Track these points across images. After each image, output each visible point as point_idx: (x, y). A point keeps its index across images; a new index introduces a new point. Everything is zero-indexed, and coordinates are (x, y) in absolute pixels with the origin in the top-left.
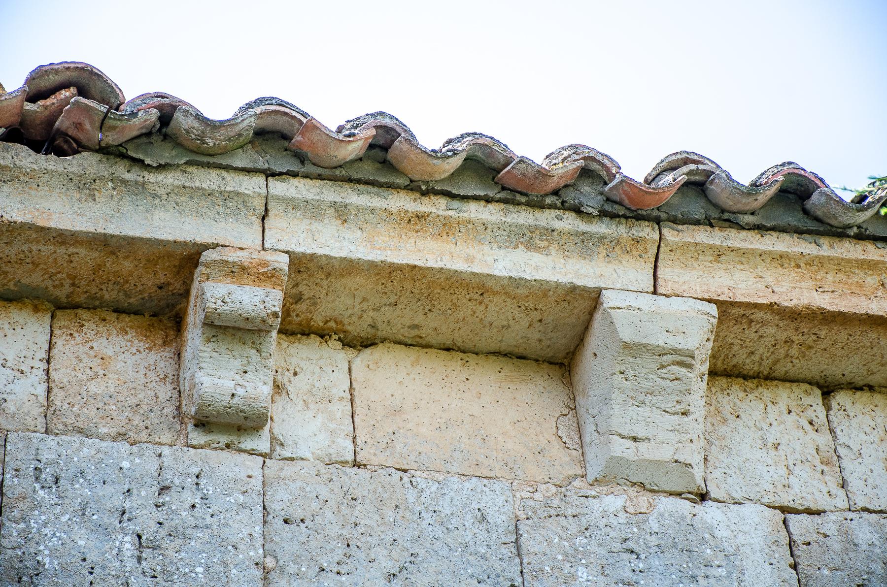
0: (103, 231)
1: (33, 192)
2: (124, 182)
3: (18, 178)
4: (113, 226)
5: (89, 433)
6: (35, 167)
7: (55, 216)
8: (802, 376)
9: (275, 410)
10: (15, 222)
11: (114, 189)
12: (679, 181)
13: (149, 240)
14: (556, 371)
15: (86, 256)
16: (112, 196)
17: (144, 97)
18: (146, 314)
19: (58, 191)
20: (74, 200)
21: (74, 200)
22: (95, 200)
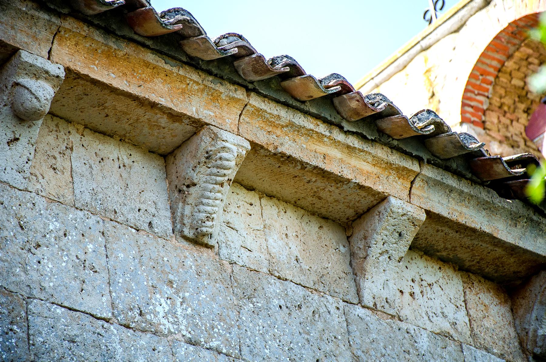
0: (518, 245)
1: (493, 217)
2: (532, 220)
3: (490, 209)
4: (521, 243)
5: (490, 351)
6: (500, 204)
7: (500, 232)
8: (65, 116)
9: (20, 138)
10: (485, 232)
11: (526, 222)
12: (476, 132)
13: (534, 253)
14: (161, 161)
15: (486, 247)
16: (524, 226)
17: (247, 49)
18: (495, 282)
19: (503, 218)
20: (508, 224)
21: (508, 224)
22: (516, 226)
